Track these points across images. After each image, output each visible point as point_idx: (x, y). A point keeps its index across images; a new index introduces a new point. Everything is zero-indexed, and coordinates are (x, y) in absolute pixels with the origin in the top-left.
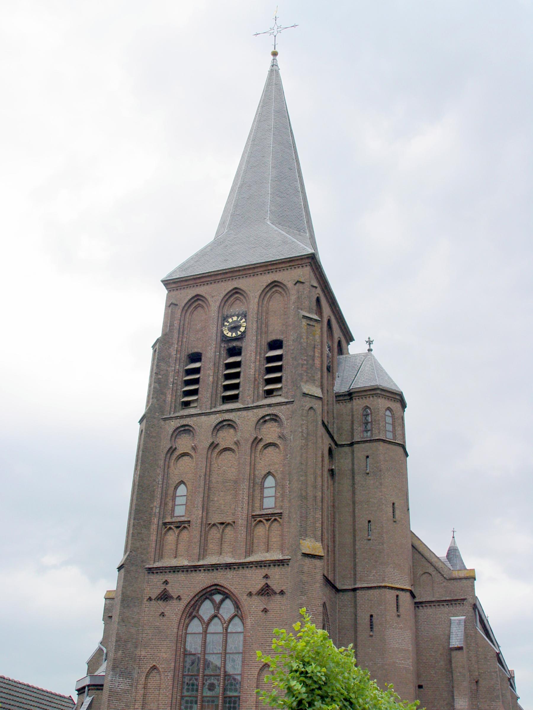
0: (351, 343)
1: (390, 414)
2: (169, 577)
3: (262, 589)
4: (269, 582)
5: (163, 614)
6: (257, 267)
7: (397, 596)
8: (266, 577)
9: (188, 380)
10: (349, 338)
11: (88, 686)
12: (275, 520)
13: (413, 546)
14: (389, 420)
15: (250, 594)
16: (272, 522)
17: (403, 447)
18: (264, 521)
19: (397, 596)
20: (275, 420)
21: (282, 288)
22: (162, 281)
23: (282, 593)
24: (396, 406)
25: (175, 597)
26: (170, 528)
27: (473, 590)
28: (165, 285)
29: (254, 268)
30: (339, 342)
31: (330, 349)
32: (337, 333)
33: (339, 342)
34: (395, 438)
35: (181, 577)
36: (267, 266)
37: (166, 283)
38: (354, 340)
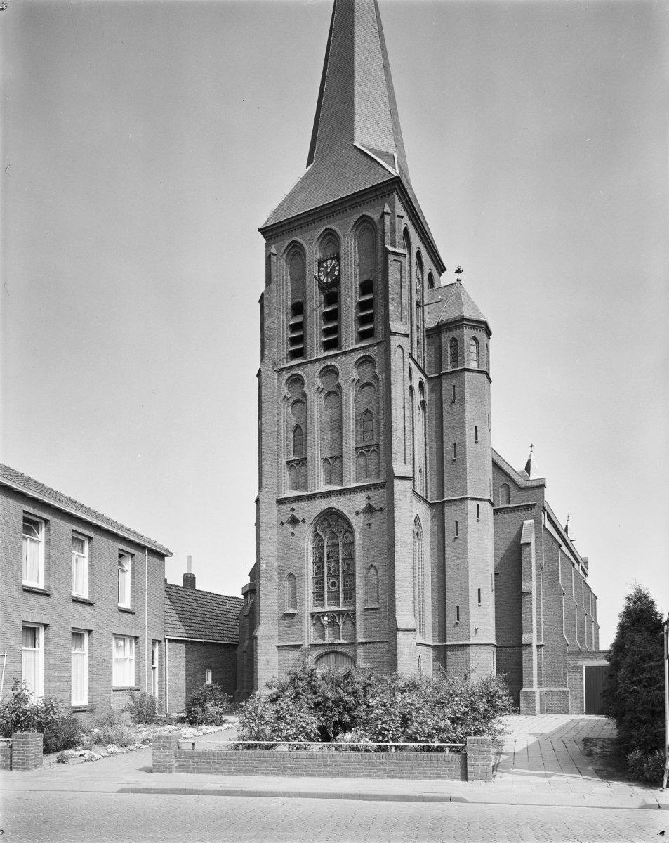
0: (443, 274)
1: (475, 343)
2: (294, 505)
3: (366, 508)
4: (371, 502)
5: (293, 534)
6: (312, 214)
7: (478, 505)
8: (293, 509)
9: (362, 316)
10: (441, 269)
11: (249, 591)
12: (374, 450)
13: (495, 464)
14: (474, 349)
15: (357, 513)
16: (372, 452)
17: (487, 374)
18: (365, 452)
19: (478, 505)
20: (370, 362)
21: (371, 223)
22: (259, 230)
23: (304, 521)
24: (480, 335)
25: (301, 520)
26: (292, 466)
27: (543, 497)
28: (262, 234)
29: (342, 203)
30: (430, 275)
31: (421, 282)
32: (428, 264)
33: (430, 275)
34: (478, 366)
35: (305, 504)
36: (354, 199)
37: (263, 231)
38: (446, 270)
